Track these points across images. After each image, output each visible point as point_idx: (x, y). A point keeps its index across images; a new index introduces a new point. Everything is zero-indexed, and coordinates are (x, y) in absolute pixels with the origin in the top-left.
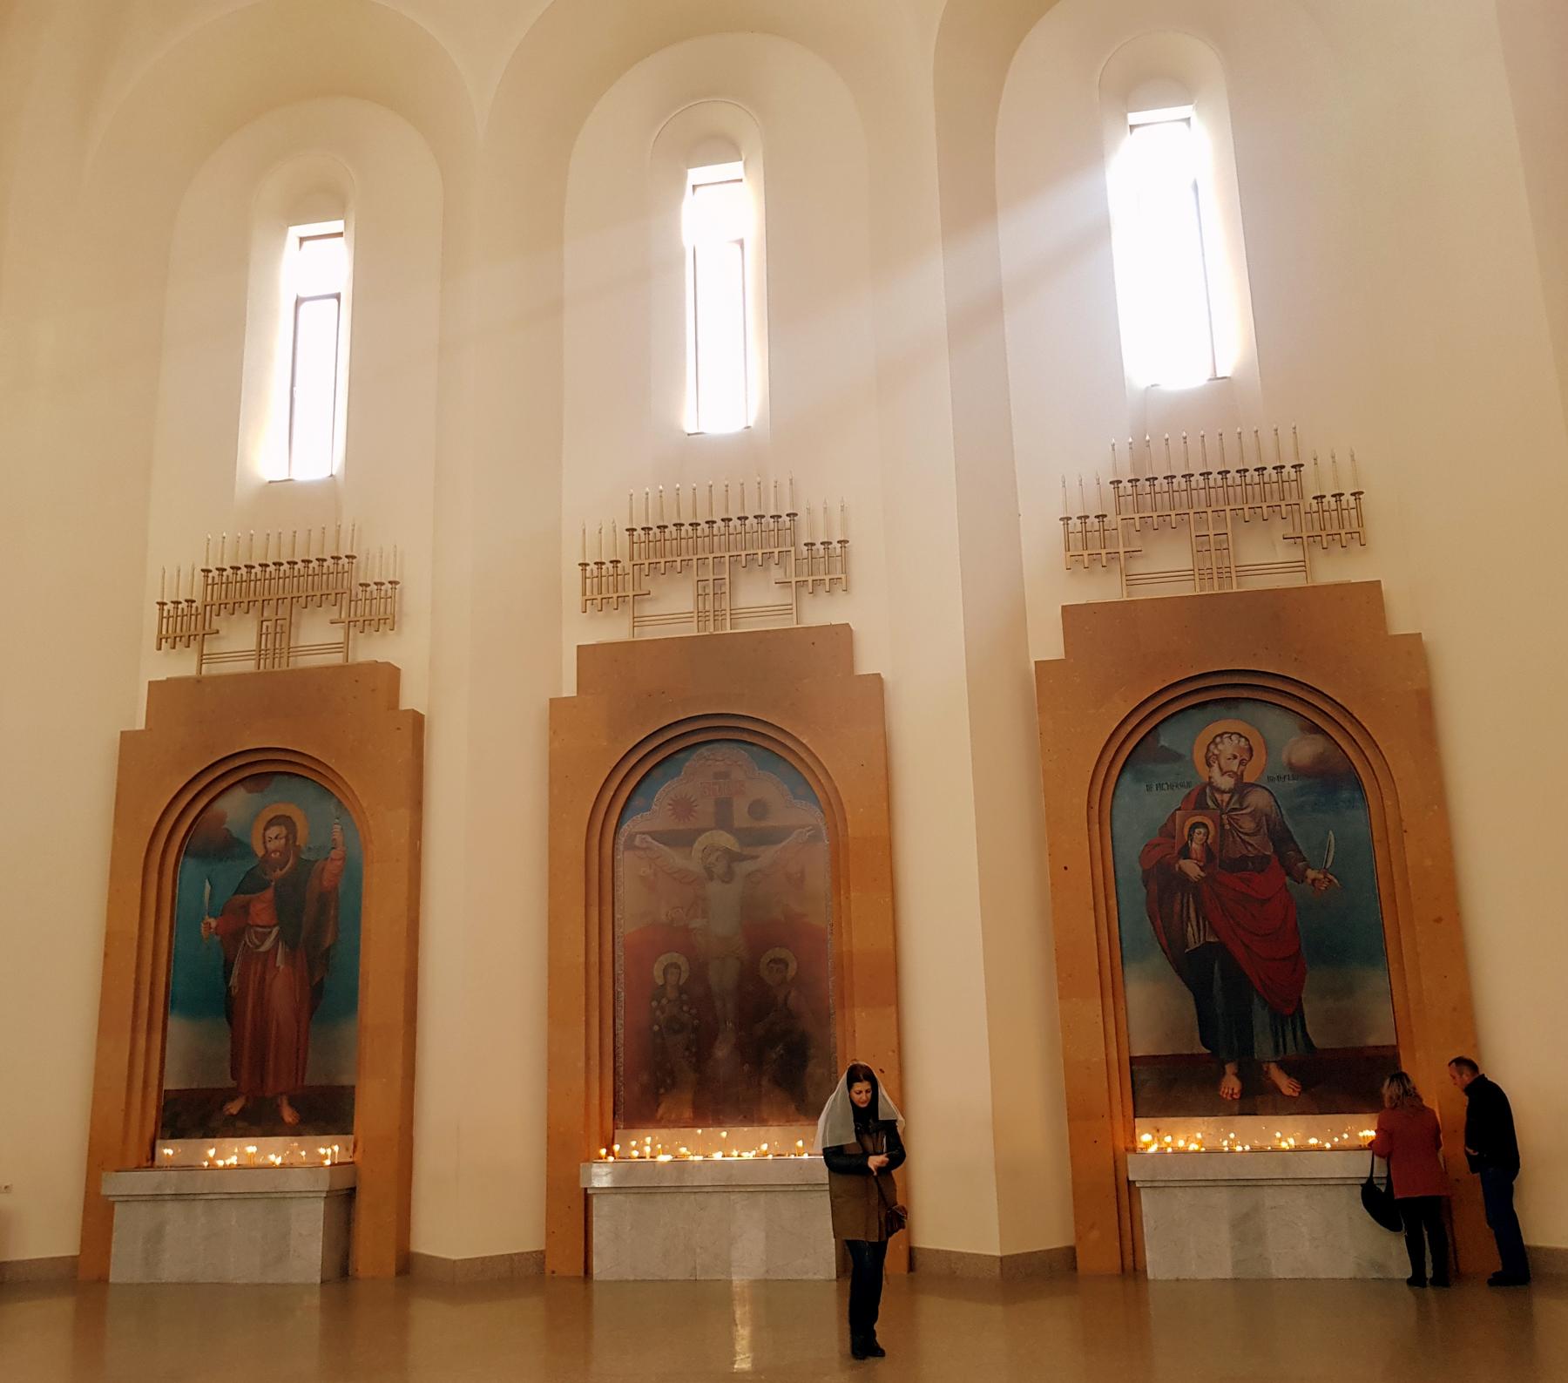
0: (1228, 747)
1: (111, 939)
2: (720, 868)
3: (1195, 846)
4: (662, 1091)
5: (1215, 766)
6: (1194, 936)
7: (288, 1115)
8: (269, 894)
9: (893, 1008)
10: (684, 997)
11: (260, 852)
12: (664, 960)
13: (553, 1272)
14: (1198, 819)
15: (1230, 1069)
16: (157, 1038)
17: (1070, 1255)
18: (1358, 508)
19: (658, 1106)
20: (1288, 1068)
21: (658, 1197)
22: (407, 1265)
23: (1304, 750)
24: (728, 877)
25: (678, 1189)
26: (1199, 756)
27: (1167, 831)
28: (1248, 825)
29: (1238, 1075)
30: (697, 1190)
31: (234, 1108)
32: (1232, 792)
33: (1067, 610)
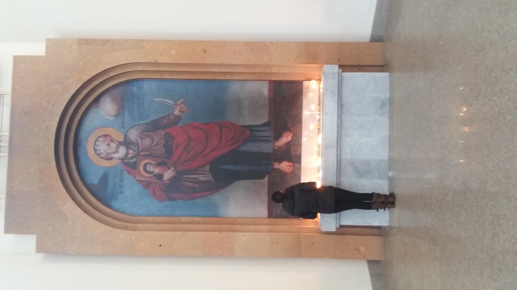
0: (103, 148)
3: (157, 171)
6: (205, 177)
15: (277, 166)
17: (371, 263)
20: (277, 137)
26: (106, 164)
27: (147, 185)
28: (147, 142)
29: (280, 161)
32: (128, 148)
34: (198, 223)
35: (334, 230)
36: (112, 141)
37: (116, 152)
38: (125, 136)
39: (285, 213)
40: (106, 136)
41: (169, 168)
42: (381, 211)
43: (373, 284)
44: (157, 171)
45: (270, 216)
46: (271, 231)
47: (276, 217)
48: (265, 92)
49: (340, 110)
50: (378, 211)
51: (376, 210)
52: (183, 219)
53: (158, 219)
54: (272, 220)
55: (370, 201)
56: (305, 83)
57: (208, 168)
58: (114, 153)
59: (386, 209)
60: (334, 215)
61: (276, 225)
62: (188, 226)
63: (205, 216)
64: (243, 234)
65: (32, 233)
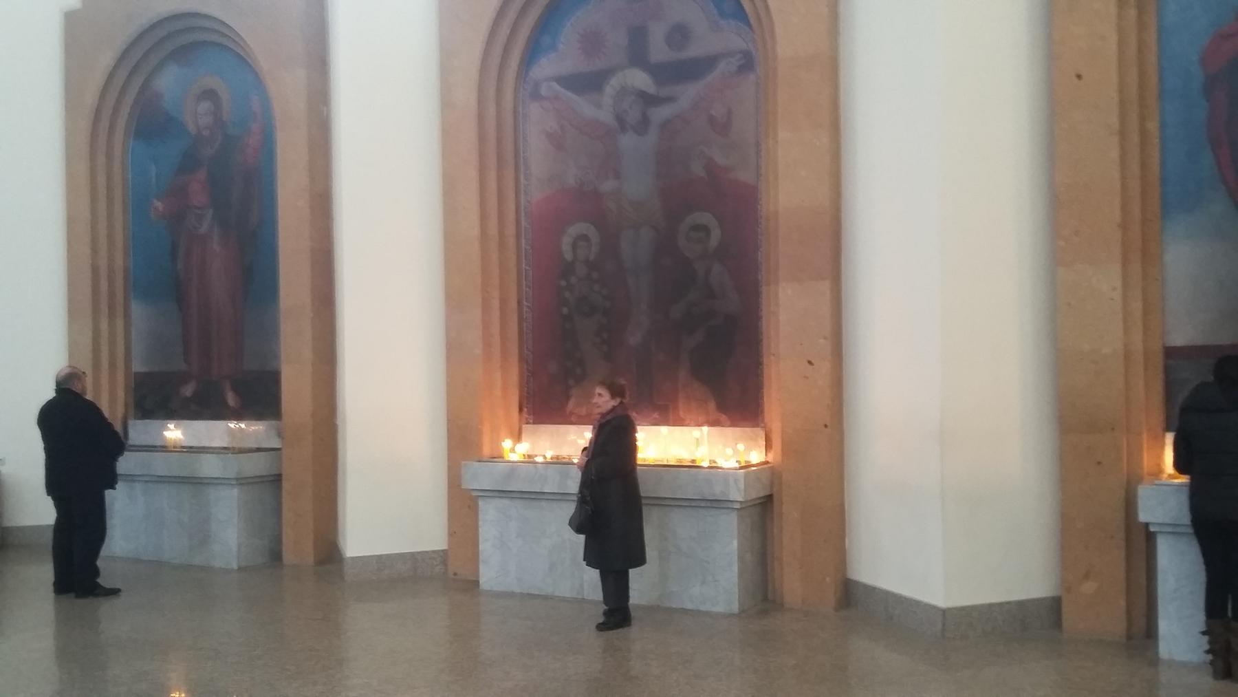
1: (71, 222)
2: (633, 116)
4: (571, 382)
7: (231, 399)
9: (825, 286)
10: (595, 275)
11: (192, 128)
12: (574, 230)
13: (455, 574)
16: (120, 323)
17: (1054, 607)
19: (568, 398)
21: (544, 504)
24: (643, 125)
34: (1144, 166)
35: (1143, 517)
39: (1181, 398)
42: (1204, 642)
43: (1001, 605)
45: (1171, 353)
46: (1127, 356)
47: (1167, 370)
50: (1204, 633)
51: (1204, 628)
52: (1153, 126)
53: (1152, 59)
54: (1159, 361)
55: (1230, 614)
59: (1210, 657)
60: (1186, 518)
61: (1146, 369)
62: (1135, 138)
63: (1164, 181)
64: (1118, 284)
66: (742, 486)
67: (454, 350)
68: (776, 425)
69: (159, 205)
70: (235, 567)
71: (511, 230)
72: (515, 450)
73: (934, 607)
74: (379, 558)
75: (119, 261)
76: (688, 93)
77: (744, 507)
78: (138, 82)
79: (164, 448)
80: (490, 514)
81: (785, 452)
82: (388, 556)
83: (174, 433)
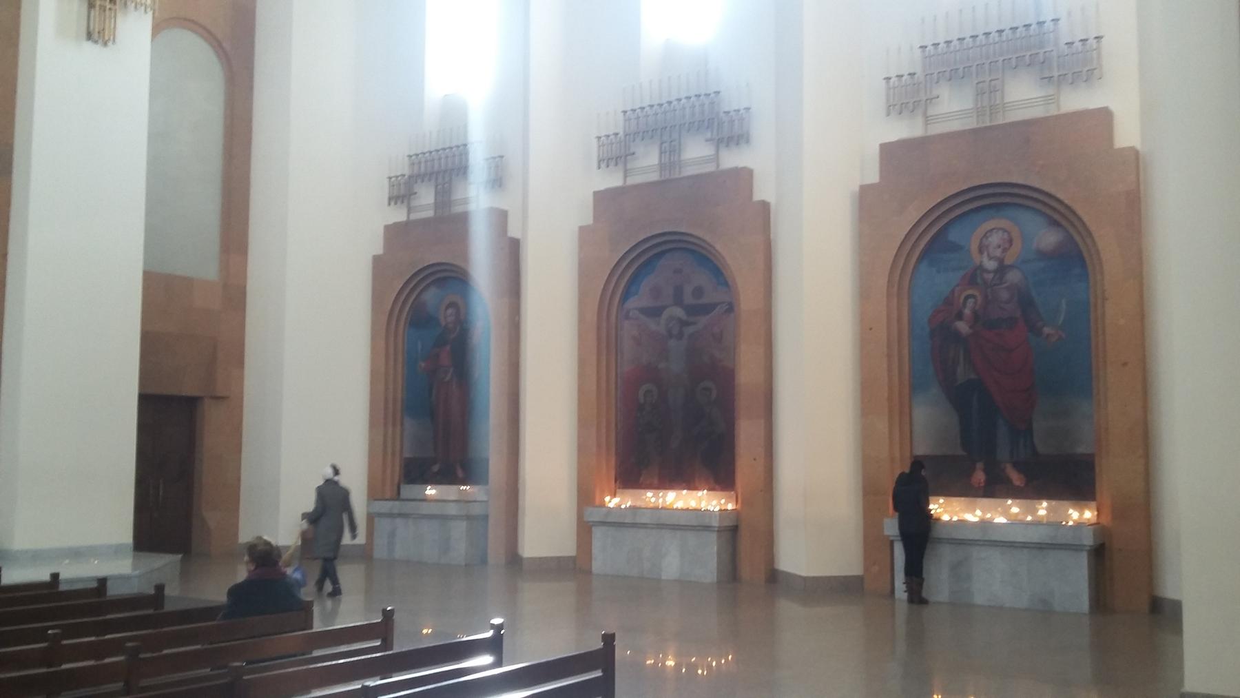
0: (995, 239)
3: (967, 311)
5: (985, 254)
6: (962, 373)
8: (448, 347)
11: (443, 324)
12: (645, 388)
14: (970, 292)
15: (980, 465)
16: (399, 427)
18: (1098, 49)
20: (1016, 465)
22: (773, 577)
23: (1049, 239)
24: (680, 336)
25: (634, 525)
26: (974, 247)
27: (949, 301)
28: (1004, 295)
29: (986, 471)
30: (644, 526)
31: (436, 468)
32: (996, 271)
33: (596, 193)
36: (1005, 250)
37: (990, 258)
38: (1011, 267)
40: (1011, 241)
41: (970, 327)
44: (967, 311)
48: (1081, 450)
49: (1033, 545)
50: (904, 583)
51: (904, 581)
56: (1093, 504)
57: (973, 376)
58: (988, 255)
65: (882, 177)
66: (718, 518)
67: (582, 449)
68: (740, 491)
69: (423, 365)
70: (463, 563)
71: (613, 386)
72: (612, 502)
73: (800, 577)
74: (540, 558)
75: (399, 396)
76: (703, 320)
77: (720, 531)
78: (414, 296)
79: (425, 500)
80: (598, 533)
81: (742, 503)
82: (546, 558)
83: (430, 491)
